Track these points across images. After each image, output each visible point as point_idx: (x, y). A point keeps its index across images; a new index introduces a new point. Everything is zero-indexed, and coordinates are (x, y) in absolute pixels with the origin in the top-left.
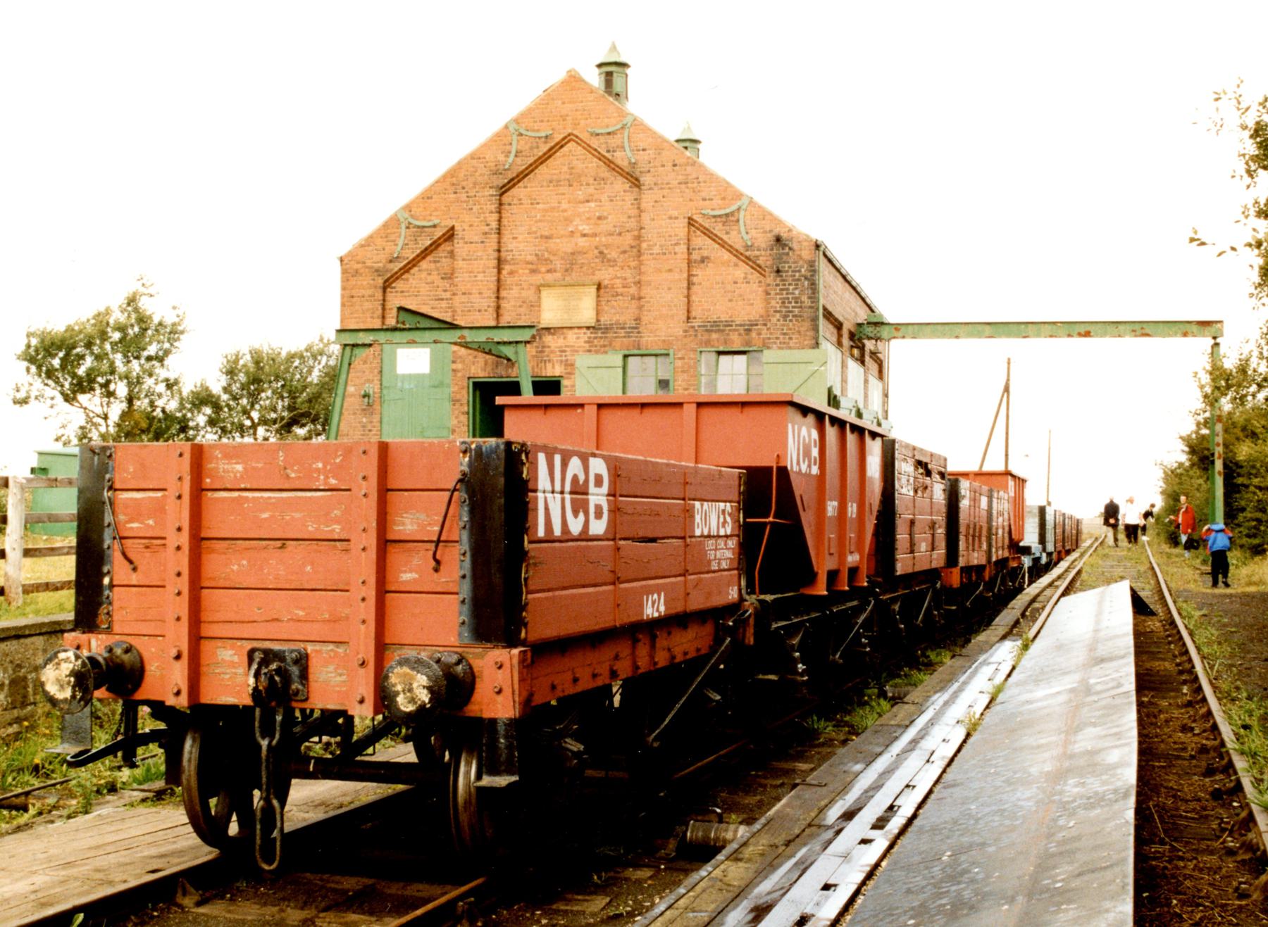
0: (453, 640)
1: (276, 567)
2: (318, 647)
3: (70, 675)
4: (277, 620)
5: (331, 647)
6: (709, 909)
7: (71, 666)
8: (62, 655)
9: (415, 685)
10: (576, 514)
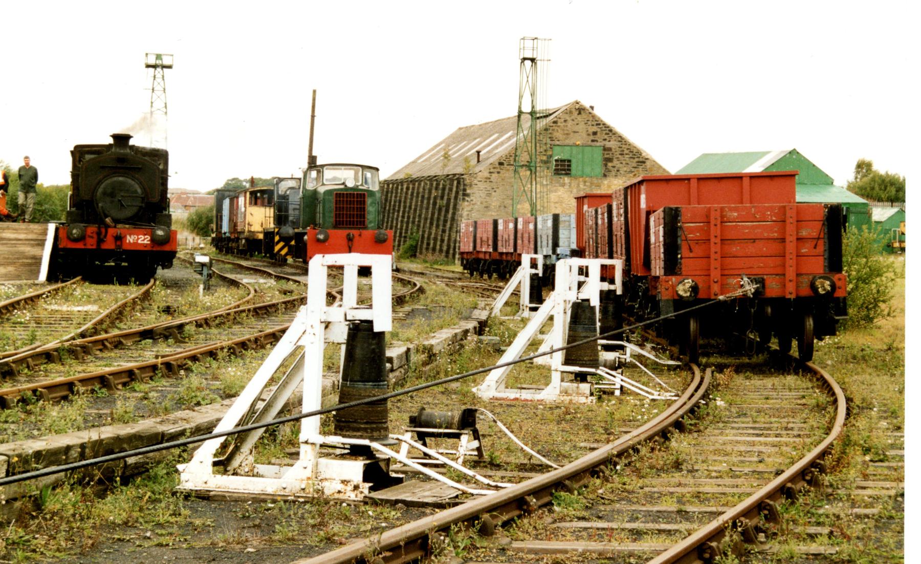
0: (822, 271)
1: (751, 249)
6: (391, 375)
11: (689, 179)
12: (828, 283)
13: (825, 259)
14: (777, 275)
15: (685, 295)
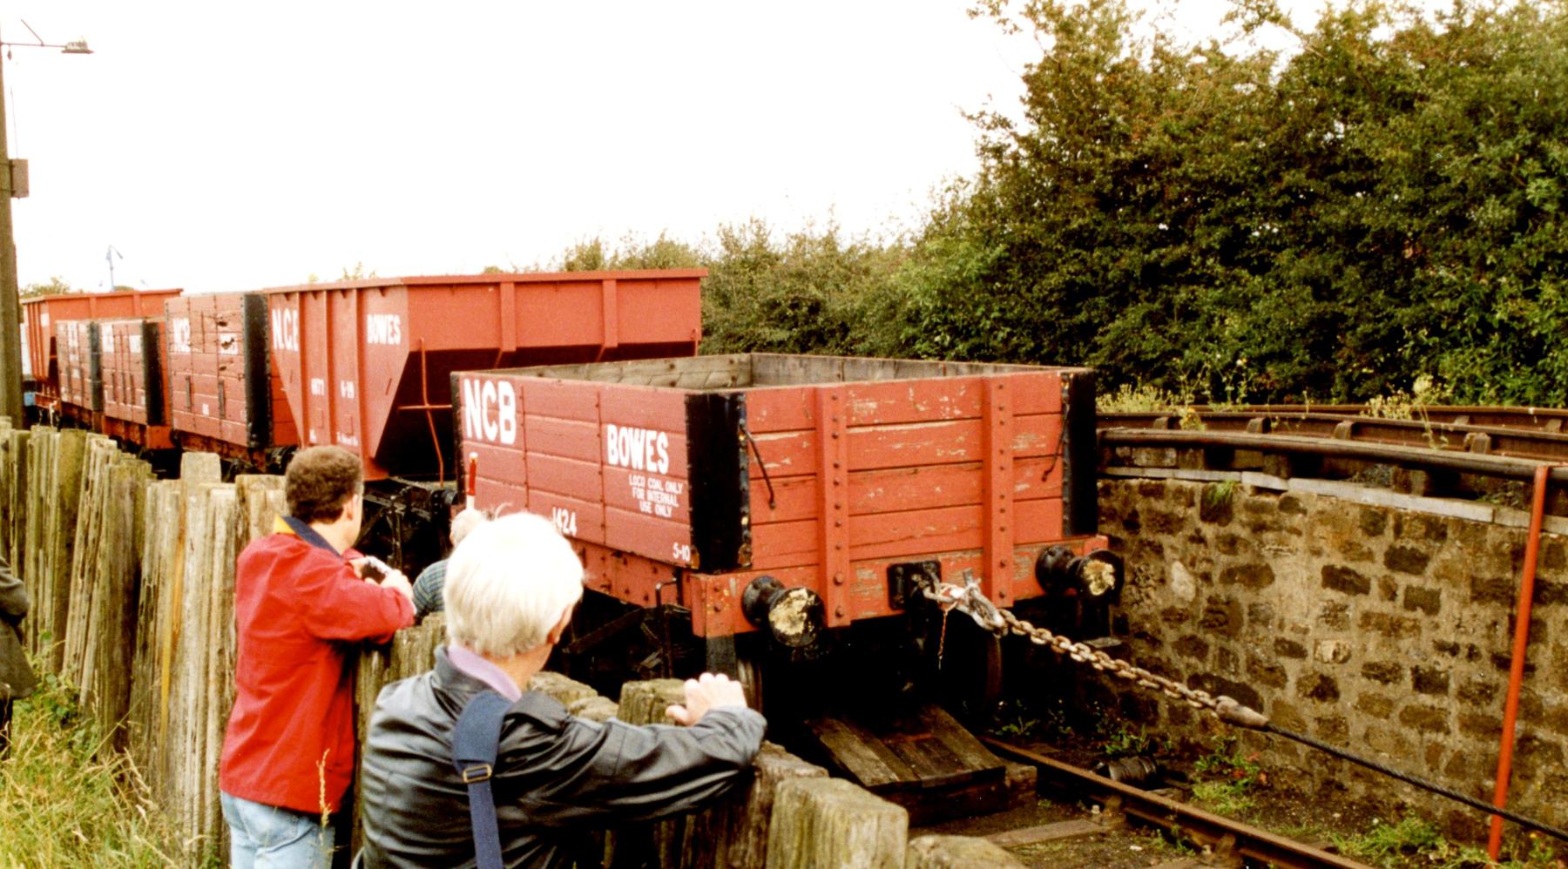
1: (909, 490)
2: (947, 556)
3: (803, 611)
4: (911, 537)
5: (959, 554)
7: (803, 603)
8: (793, 594)
9: (1104, 573)
10: (491, 424)
11: (497, 285)
12: (1109, 568)
13: (1065, 504)
14: (965, 550)
15: (791, 632)
